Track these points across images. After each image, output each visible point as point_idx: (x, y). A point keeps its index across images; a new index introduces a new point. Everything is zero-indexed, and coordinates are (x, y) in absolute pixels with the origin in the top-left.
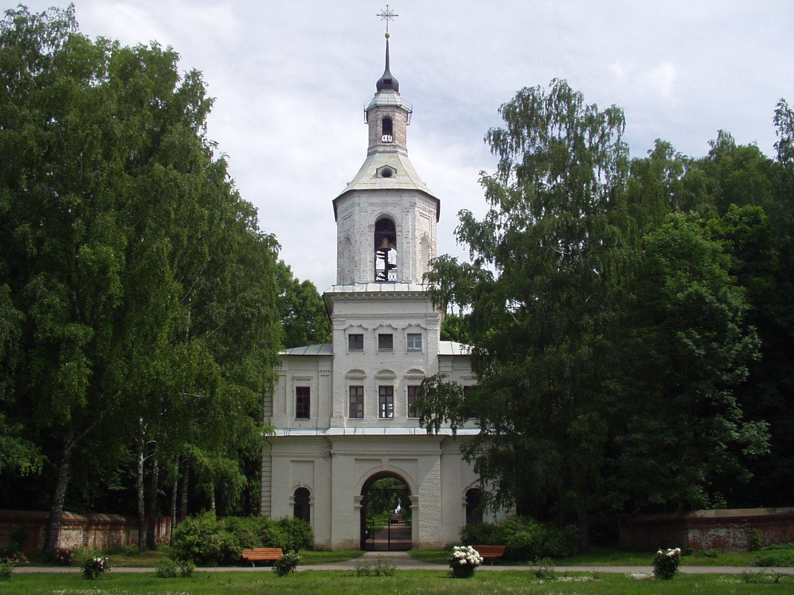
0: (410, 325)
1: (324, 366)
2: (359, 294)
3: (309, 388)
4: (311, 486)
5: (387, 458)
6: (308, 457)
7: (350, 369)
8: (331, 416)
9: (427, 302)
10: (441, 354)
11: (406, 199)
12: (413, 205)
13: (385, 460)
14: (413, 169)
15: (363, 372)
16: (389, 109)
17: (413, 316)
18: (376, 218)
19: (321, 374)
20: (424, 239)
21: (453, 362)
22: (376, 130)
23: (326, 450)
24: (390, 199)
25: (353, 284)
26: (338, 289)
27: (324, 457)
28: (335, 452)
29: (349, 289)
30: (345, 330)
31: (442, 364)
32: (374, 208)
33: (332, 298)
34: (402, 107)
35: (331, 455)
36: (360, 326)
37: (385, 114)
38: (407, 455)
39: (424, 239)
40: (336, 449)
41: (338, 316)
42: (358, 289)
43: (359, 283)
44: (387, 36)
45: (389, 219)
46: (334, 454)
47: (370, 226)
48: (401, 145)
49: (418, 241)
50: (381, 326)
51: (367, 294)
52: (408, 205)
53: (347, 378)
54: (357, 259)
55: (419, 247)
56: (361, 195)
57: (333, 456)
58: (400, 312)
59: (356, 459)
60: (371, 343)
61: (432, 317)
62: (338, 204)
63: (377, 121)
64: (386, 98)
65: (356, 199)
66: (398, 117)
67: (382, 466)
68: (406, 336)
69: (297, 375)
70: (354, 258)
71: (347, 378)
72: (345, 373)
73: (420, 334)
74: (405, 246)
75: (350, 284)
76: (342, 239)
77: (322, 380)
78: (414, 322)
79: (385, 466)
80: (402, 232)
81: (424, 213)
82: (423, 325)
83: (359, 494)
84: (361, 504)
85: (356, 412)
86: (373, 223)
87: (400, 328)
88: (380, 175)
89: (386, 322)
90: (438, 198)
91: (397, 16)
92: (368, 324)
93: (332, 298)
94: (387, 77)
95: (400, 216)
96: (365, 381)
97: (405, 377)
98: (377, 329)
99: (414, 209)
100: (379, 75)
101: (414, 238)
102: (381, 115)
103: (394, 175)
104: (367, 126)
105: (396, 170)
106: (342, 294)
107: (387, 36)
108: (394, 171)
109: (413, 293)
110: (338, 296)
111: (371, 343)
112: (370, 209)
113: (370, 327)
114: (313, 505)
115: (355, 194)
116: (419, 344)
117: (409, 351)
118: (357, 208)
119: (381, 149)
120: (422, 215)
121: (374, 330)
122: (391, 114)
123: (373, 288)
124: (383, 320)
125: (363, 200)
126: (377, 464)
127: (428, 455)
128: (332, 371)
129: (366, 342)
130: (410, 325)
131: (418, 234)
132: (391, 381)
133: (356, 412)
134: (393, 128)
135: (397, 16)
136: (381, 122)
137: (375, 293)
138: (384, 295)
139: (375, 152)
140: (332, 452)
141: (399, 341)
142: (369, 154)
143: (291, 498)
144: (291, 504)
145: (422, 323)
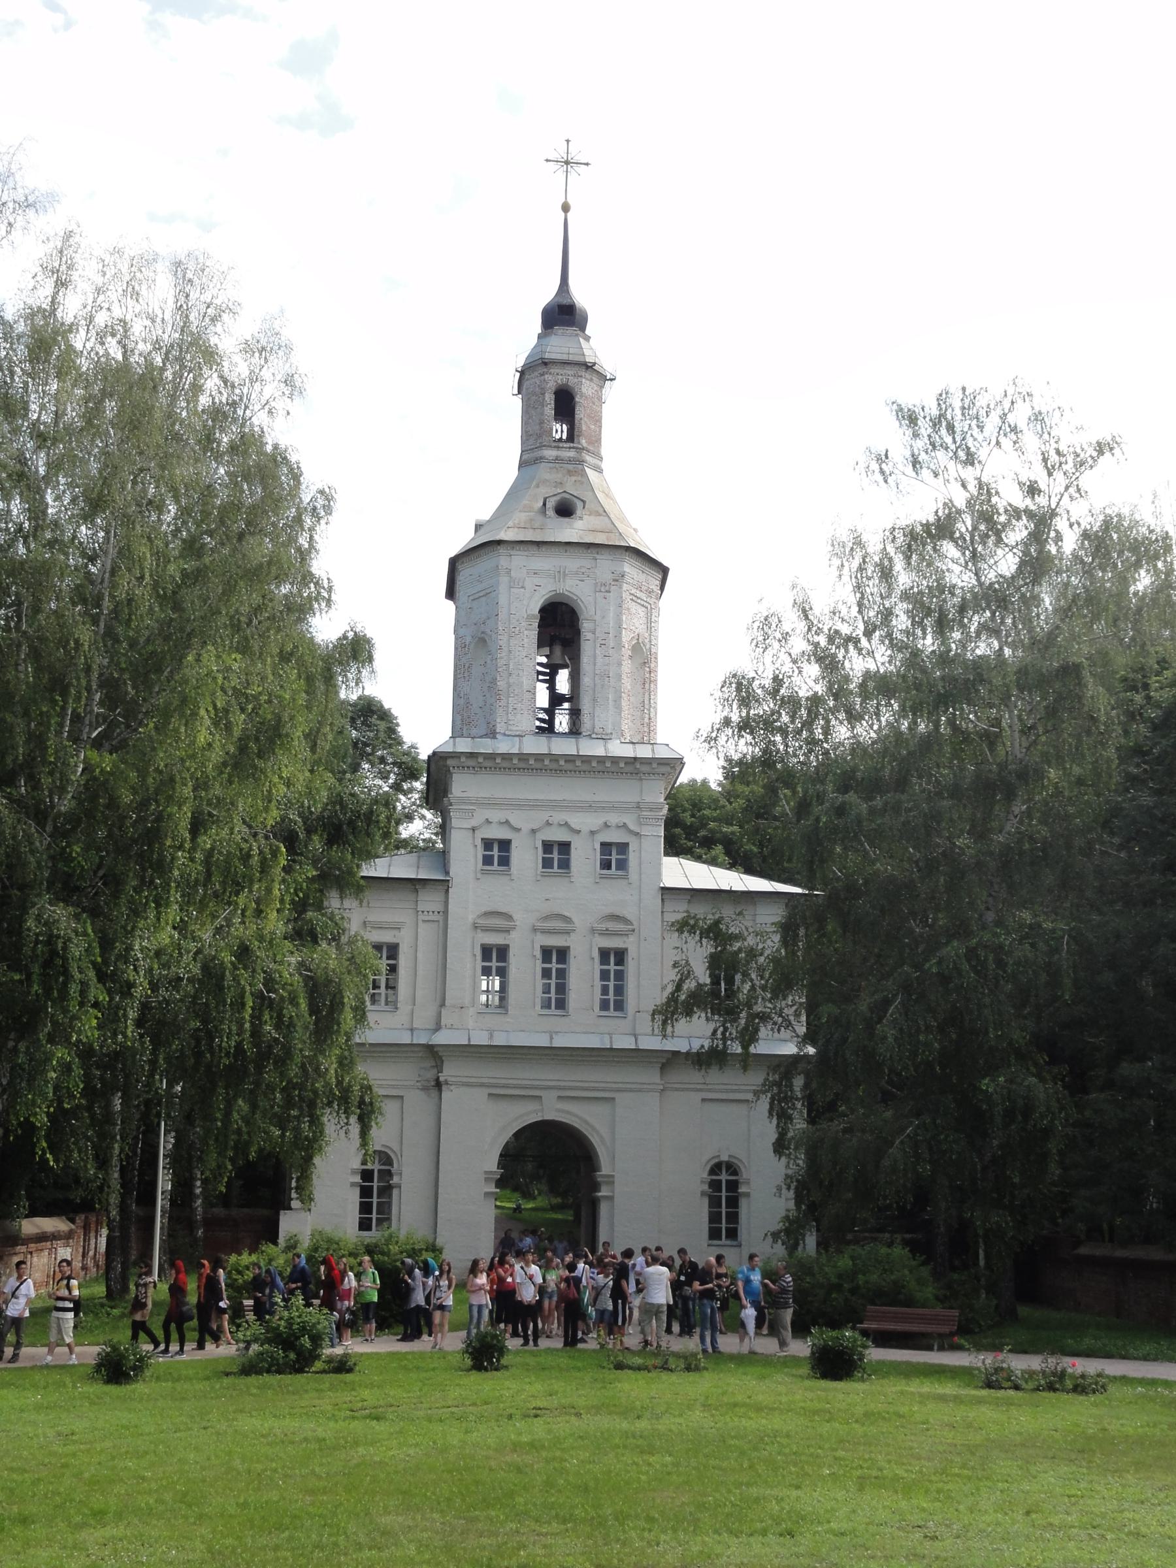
0: (606, 825)
1: (429, 901)
2: (507, 757)
3: (508, 946)
4: (396, 1147)
5: (556, 1093)
6: (393, 1087)
7: (483, 910)
8: (443, 1005)
9: (641, 779)
10: (668, 885)
11: (605, 565)
12: (619, 578)
13: (549, 1097)
14: (615, 502)
15: (509, 917)
16: (570, 371)
17: (613, 808)
18: (542, 601)
19: (421, 917)
20: (637, 648)
21: (689, 902)
22: (542, 414)
23: (431, 1074)
24: (573, 562)
25: (492, 734)
26: (464, 746)
27: (425, 1089)
28: (449, 1079)
29: (486, 746)
30: (473, 830)
31: (669, 906)
32: (537, 581)
33: (450, 762)
34: (596, 367)
35: (438, 1085)
36: (507, 822)
37: (561, 380)
38: (604, 1090)
39: (637, 648)
40: (449, 1072)
41: (463, 801)
42: (503, 746)
43: (505, 735)
44: (566, 208)
45: (561, 604)
46: (447, 1083)
47: (530, 617)
48: (591, 448)
49: (626, 652)
50: (548, 824)
51: (523, 757)
52: (608, 577)
53: (476, 927)
54: (501, 684)
55: (627, 666)
56: (512, 552)
57: (444, 1088)
58: (588, 797)
59: (490, 1095)
60: (525, 856)
61: (651, 810)
62: (459, 567)
63: (543, 394)
64: (560, 345)
65: (502, 559)
66: (585, 388)
67: (542, 1110)
68: (598, 847)
69: (372, 917)
70: (494, 681)
71: (476, 927)
72: (471, 918)
73: (627, 845)
74: (600, 660)
75: (486, 736)
76: (468, 639)
77: (423, 929)
78: (614, 819)
79: (552, 1110)
80: (594, 633)
81: (639, 594)
82: (632, 827)
83: (495, 1168)
84: (497, 1187)
85: (558, 999)
86: (536, 611)
87: (585, 829)
88: (551, 512)
89: (559, 817)
90: (665, 564)
91: (587, 164)
92: (584, 821)
93: (450, 762)
94: (565, 302)
95: (591, 599)
96: (514, 935)
97: (593, 931)
98: (479, 827)
99: (621, 587)
100: (548, 293)
101: (619, 646)
102: (553, 380)
103: (579, 512)
104: (518, 402)
105: (584, 502)
106: (472, 755)
107: (566, 208)
108: (579, 504)
109: (615, 760)
110: (463, 759)
111: (525, 856)
112: (530, 583)
113: (526, 827)
114: (610, 1198)
115: (502, 550)
116: (622, 865)
117: (602, 877)
118: (504, 580)
119: (550, 453)
120: (635, 599)
121: (534, 831)
122: (572, 381)
123: (536, 745)
124: (551, 813)
125: (518, 563)
126: (531, 1106)
127: (631, 1090)
128: (446, 912)
129: (515, 855)
130: (606, 825)
131: (626, 637)
132: (565, 937)
133: (558, 999)
134: (577, 412)
135: (587, 164)
136: (553, 397)
137: (539, 757)
138: (557, 761)
139: (538, 460)
140: (441, 1079)
141: (584, 857)
142: (523, 464)
143: (354, 1172)
144: (353, 1184)
145: (630, 821)
